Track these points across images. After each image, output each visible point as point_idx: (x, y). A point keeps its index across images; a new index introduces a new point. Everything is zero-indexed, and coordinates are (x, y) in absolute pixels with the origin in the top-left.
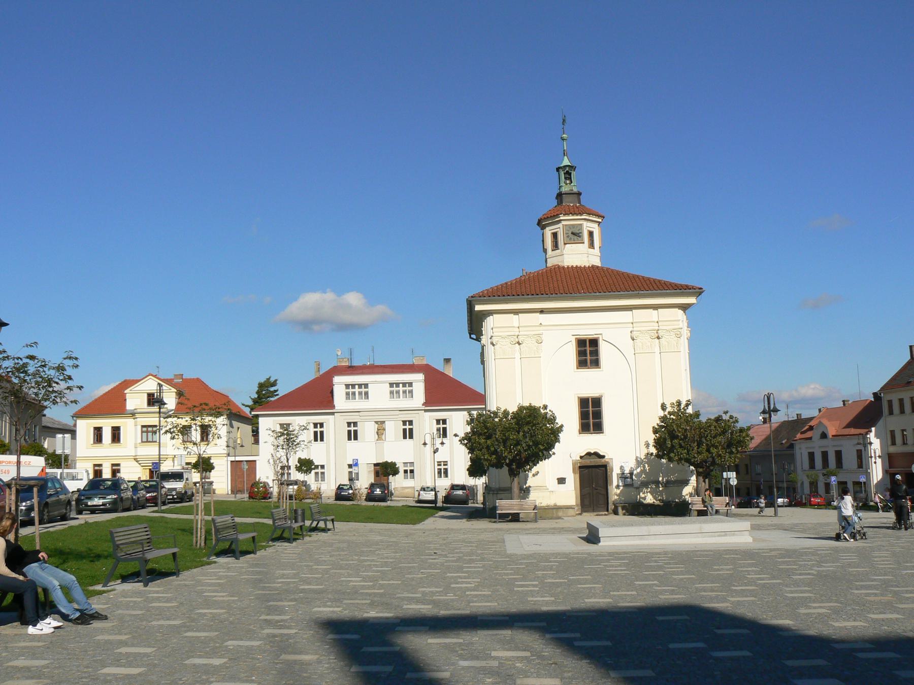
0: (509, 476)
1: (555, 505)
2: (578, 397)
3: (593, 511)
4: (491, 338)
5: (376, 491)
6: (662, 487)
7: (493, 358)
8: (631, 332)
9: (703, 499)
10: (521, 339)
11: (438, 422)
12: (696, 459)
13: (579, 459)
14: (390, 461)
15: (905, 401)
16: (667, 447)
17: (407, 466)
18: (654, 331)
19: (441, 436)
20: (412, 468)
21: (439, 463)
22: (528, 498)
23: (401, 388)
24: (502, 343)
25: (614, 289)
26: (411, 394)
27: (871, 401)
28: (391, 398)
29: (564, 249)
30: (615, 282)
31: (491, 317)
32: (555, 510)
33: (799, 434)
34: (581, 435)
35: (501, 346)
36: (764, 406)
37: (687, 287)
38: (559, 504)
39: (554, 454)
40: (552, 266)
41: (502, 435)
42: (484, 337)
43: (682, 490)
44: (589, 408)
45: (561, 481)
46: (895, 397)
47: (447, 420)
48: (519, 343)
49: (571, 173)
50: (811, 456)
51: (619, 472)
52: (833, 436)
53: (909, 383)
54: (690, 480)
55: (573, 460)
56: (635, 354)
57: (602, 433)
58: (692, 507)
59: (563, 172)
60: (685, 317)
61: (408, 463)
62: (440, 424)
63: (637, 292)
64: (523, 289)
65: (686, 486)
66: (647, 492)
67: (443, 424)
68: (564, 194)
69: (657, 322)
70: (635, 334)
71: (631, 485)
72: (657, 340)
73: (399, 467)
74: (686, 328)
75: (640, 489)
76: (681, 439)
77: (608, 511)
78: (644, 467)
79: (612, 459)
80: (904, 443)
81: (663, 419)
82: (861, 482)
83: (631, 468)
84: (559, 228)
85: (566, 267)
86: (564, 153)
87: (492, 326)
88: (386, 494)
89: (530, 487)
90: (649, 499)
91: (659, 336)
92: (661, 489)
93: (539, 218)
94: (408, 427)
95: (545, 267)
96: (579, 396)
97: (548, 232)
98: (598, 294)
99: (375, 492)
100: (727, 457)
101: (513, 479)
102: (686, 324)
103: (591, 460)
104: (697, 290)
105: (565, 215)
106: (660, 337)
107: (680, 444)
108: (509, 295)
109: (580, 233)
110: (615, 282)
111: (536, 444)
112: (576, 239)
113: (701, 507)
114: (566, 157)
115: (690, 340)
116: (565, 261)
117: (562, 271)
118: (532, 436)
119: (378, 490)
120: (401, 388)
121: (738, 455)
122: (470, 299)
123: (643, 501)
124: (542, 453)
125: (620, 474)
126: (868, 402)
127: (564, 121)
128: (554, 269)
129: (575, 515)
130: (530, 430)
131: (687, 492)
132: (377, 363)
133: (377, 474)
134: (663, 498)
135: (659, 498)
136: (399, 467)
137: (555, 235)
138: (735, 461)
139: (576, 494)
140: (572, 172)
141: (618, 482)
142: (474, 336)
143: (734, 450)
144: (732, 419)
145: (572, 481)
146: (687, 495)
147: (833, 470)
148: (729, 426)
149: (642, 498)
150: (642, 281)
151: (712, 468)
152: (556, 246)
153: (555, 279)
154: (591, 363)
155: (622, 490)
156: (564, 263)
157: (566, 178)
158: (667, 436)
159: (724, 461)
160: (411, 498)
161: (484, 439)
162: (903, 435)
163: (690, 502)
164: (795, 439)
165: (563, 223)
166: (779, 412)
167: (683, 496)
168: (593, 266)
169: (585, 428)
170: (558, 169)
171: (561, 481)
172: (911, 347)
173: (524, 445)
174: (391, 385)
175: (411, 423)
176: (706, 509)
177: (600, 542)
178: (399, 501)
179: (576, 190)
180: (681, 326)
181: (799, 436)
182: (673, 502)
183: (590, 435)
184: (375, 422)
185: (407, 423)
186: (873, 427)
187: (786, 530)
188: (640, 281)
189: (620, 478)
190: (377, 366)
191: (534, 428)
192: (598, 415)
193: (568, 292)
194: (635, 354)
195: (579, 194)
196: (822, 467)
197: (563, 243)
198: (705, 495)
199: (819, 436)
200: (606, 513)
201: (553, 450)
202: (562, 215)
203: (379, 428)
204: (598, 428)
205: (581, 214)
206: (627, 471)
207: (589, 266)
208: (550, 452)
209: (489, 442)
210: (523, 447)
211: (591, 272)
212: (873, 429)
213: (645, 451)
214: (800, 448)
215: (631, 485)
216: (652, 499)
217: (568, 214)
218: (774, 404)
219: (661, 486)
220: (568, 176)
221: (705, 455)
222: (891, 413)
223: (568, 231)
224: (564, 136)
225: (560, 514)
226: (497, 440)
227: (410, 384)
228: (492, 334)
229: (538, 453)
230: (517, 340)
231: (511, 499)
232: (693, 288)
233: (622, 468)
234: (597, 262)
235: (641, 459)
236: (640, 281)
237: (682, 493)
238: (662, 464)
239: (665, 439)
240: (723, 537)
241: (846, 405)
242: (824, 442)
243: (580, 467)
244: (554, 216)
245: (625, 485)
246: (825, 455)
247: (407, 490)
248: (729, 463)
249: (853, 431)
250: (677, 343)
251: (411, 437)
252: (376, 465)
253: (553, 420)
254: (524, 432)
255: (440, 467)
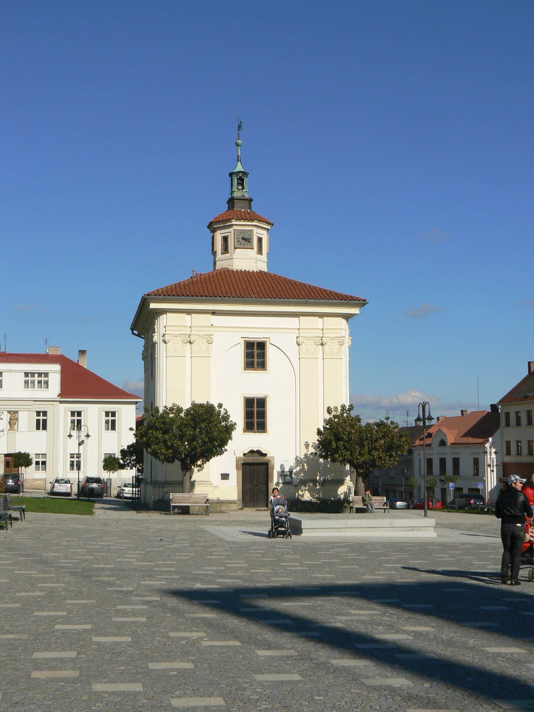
0: (181, 471)
1: (218, 500)
2: (244, 397)
3: (254, 506)
4: (163, 336)
5: (9, 482)
6: (319, 485)
7: (165, 355)
8: (297, 338)
9: (363, 498)
10: (192, 338)
11: (73, 413)
12: (359, 461)
13: (243, 456)
14: (23, 452)
15: (510, 416)
16: (332, 448)
17: (39, 458)
18: (318, 338)
19: (76, 427)
20: (44, 460)
21: (72, 456)
22: (193, 492)
23: (36, 378)
24: (173, 342)
25: (283, 296)
26: (40, 384)
27: (489, 412)
28: (25, 388)
29: (234, 253)
30: (284, 288)
31: (165, 315)
32: (218, 504)
33: (418, 440)
34: (245, 433)
35: (173, 344)
36: (419, 413)
37: (352, 298)
38: (222, 498)
39: (226, 450)
40: (222, 269)
41: (178, 430)
42: (156, 334)
43: (338, 489)
44: (254, 408)
45: (225, 477)
46: (512, 410)
47: (117, 413)
48: (190, 343)
49: (244, 179)
50: (430, 462)
51: (279, 470)
52: (451, 444)
53: (526, 397)
54: (345, 480)
55: (236, 457)
56: (299, 359)
57: (265, 432)
58: (353, 505)
59: (236, 178)
60: (347, 326)
61: (39, 454)
62: (74, 416)
63: (306, 300)
64: (197, 290)
65: (342, 485)
66: (305, 490)
67: (112, 416)
68: (236, 199)
69: (322, 330)
70: (300, 340)
71: (290, 483)
72: (321, 347)
73: (32, 458)
74: (347, 336)
75: (299, 487)
76: (346, 441)
77: (267, 506)
78: (303, 466)
79: (274, 457)
80: (519, 454)
81: (328, 422)
82: (479, 489)
83: (291, 466)
84: (230, 232)
85: (235, 271)
86: (238, 159)
87: (165, 324)
88: (19, 485)
89: (195, 481)
90: (307, 496)
91: (323, 343)
92: (318, 487)
93: (211, 220)
94: (41, 418)
95: (212, 270)
96: (245, 396)
97: (219, 236)
98: (268, 299)
99: (8, 483)
100: (388, 459)
101: (185, 474)
102: (348, 333)
103: (254, 458)
104: (361, 302)
105: (236, 220)
106: (324, 344)
107: (344, 446)
108: (183, 296)
109: (251, 239)
110: (284, 288)
111: (211, 440)
112: (246, 244)
113: (361, 506)
114: (239, 163)
115: (351, 349)
116: (234, 264)
117: (232, 274)
118: (207, 433)
119: (11, 481)
120: (36, 378)
121: (397, 459)
122: (146, 297)
123: (301, 498)
124: (216, 449)
125: (281, 472)
126: (486, 413)
127: (240, 127)
128: (224, 271)
129: (237, 509)
130: (206, 427)
131: (342, 492)
132: (8, 352)
133: (7, 464)
134: (320, 496)
135: (316, 496)
136: (32, 458)
137: (225, 239)
138: (394, 463)
139: (238, 489)
140: (245, 178)
141: (278, 479)
142: (135, 332)
143: (394, 454)
144: (393, 424)
145: (235, 476)
146: (342, 494)
147: (451, 477)
148: (390, 431)
149: (301, 495)
150: (309, 289)
151: (371, 469)
152: (225, 250)
153: (226, 282)
154: (258, 364)
155: (281, 487)
156: (233, 266)
157: (238, 184)
158: (332, 438)
159: (384, 463)
160: (41, 490)
161: (162, 434)
162: (518, 446)
163: (351, 500)
164: (414, 445)
165: (234, 228)
166: (433, 420)
167: (339, 495)
168: (261, 272)
169: (249, 427)
170: (231, 175)
171: (225, 477)
172: (529, 363)
173: (200, 441)
174: (26, 374)
175: (45, 413)
176: (366, 507)
177: (302, 533)
178: (31, 493)
179: (248, 196)
180: (343, 335)
181: (418, 442)
182: (329, 500)
183: (254, 433)
184: (8, 411)
185: (41, 413)
186: (491, 437)
187: (452, 528)
188: (307, 289)
189: (280, 475)
190: (10, 355)
191: (210, 425)
192: (262, 415)
193: (226, 295)
194: (299, 359)
195: (250, 200)
196: (439, 473)
197: (233, 248)
198: (366, 494)
199: (438, 443)
200: (266, 508)
201: (226, 447)
202: (234, 220)
203: (12, 418)
204: (262, 427)
205: (252, 220)
206: (287, 469)
207: (257, 271)
208: (223, 448)
209: (166, 436)
210: (199, 443)
211: (259, 277)
212: (490, 439)
213: (304, 451)
214: (419, 454)
215: (290, 483)
216: (310, 496)
217: (240, 220)
218: (429, 412)
219: (318, 485)
220: (240, 182)
221: (367, 457)
222: (508, 424)
223: (239, 235)
224: (239, 141)
225: (224, 508)
226: (174, 435)
227: (46, 375)
228: (164, 332)
229: (212, 449)
230: (188, 339)
231: (183, 493)
232: (357, 299)
233: (282, 466)
234: (263, 267)
235: (300, 458)
236: (307, 289)
237: (337, 492)
238: (320, 464)
239: (330, 441)
240: (411, 532)
241: (464, 415)
242: (442, 449)
243: (243, 464)
244: (226, 220)
245: (284, 483)
246: (443, 462)
247: (37, 482)
248: (388, 466)
249: (471, 440)
250: (339, 351)
251: (45, 428)
252: (6, 455)
253: (226, 418)
254: (201, 428)
255: (72, 459)
